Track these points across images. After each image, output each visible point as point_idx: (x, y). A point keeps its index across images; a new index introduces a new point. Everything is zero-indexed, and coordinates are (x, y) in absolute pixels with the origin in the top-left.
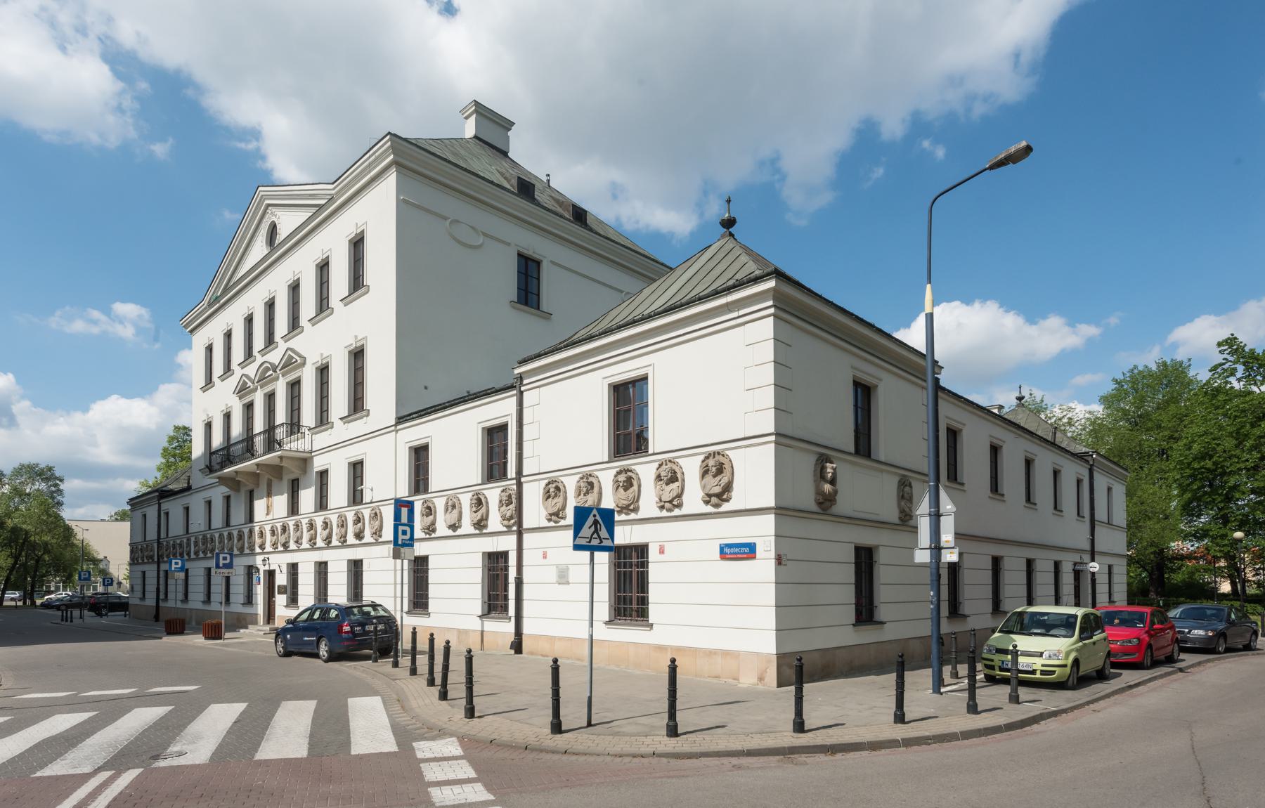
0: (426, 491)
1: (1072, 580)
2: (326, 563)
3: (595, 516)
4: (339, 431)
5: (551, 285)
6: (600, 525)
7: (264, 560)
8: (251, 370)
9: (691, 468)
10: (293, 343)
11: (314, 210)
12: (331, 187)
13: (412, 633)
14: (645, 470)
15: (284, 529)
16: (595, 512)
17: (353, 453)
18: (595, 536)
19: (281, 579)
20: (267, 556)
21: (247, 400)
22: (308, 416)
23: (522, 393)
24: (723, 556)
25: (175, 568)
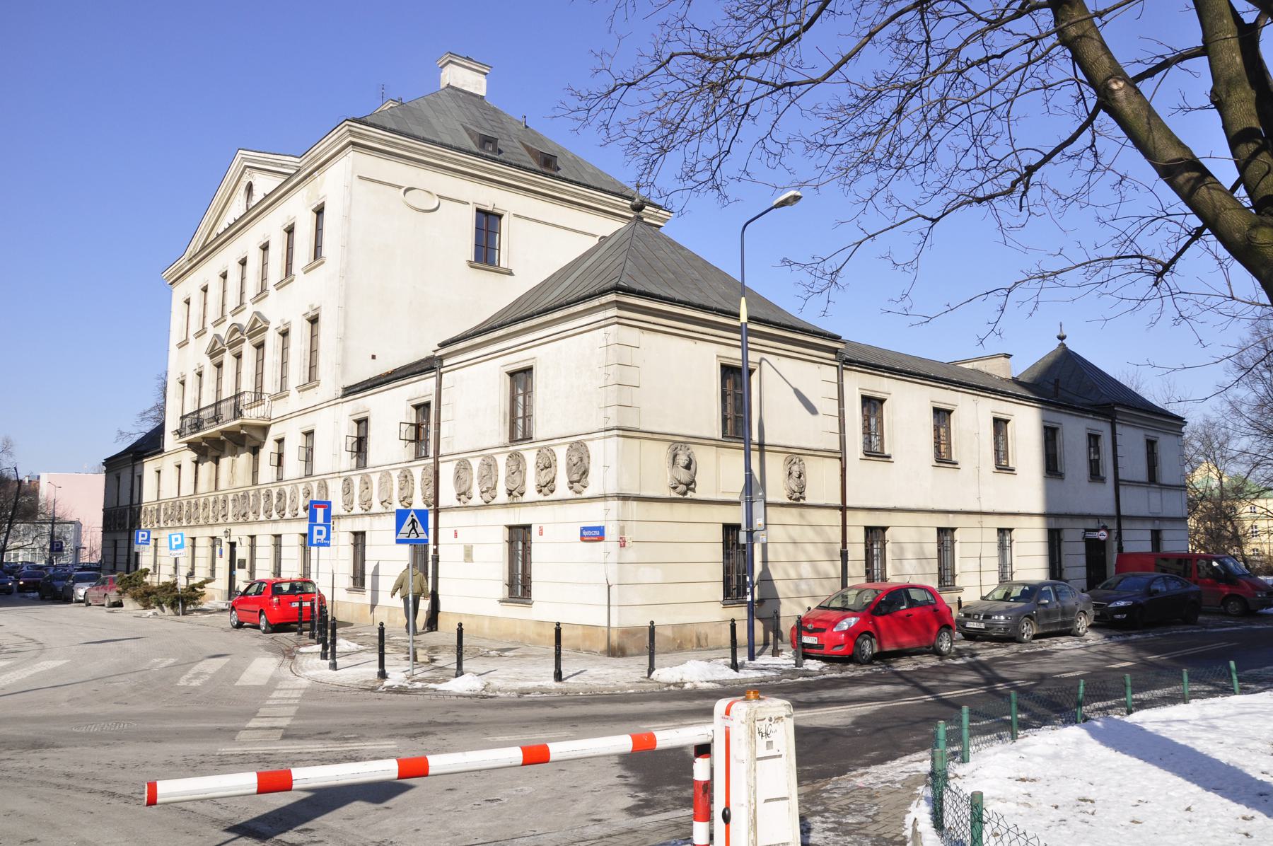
0: (365, 467)
1: (1066, 561)
4: (295, 401)
5: (510, 237)
7: (226, 532)
8: (223, 331)
9: (561, 453)
10: (259, 307)
11: (286, 177)
12: (298, 160)
13: (556, 629)
14: (530, 455)
15: (245, 497)
16: (412, 513)
17: (306, 423)
18: (413, 531)
19: (242, 553)
20: (228, 528)
21: (217, 359)
22: (270, 386)
23: (441, 374)
24: (583, 538)
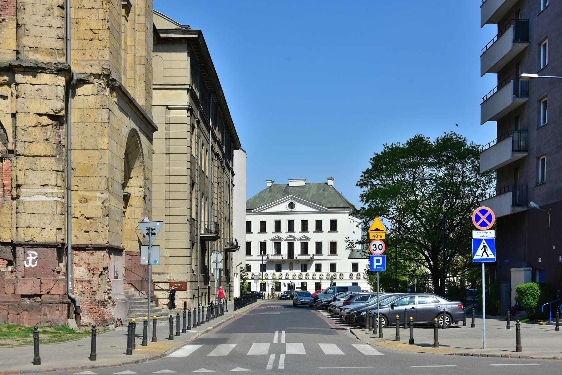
2: (306, 221)
3: (484, 243)
6: (487, 248)
18: (485, 253)
25: (377, 266)
